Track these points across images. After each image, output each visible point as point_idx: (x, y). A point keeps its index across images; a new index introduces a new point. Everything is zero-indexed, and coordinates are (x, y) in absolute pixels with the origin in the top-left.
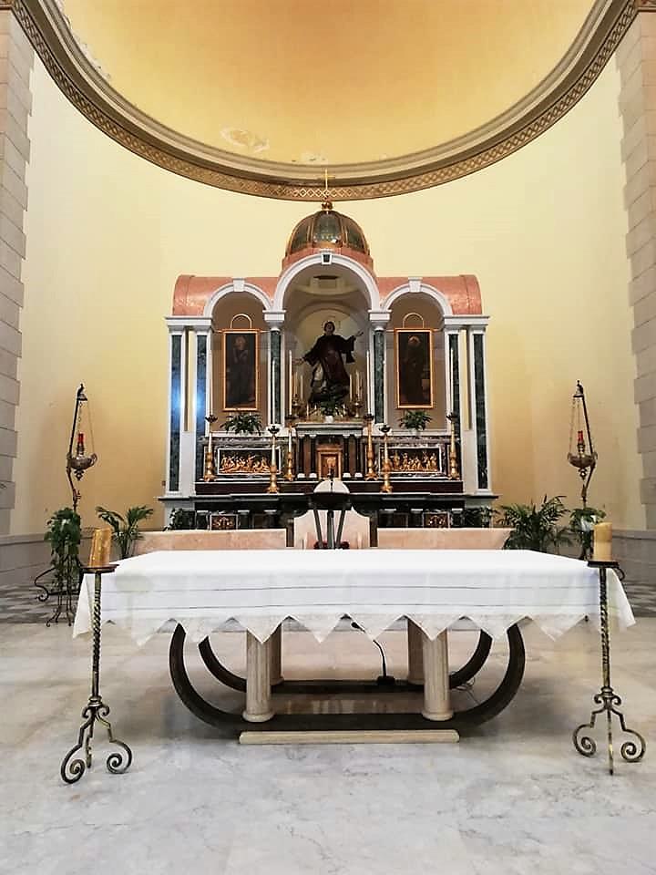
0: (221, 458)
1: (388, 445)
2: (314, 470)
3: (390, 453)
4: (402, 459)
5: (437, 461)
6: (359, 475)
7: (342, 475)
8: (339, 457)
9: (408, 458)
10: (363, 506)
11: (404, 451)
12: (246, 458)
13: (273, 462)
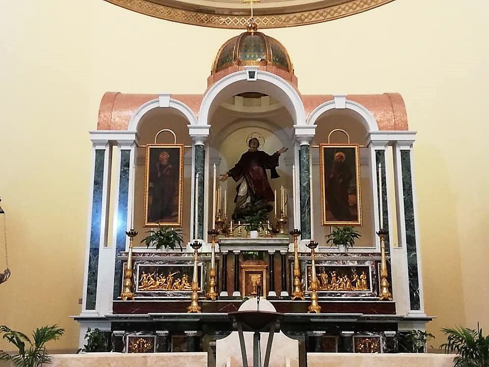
0: (141, 274)
1: (316, 262)
2: (238, 288)
3: (318, 270)
4: (330, 277)
5: (368, 280)
6: (285, 294)
7: (267, 294)
8: (264, 274)
9: (336, 277)
10: (292, 327)
11: (333, 268)
12: (166, 276)
13: (195, 279)
